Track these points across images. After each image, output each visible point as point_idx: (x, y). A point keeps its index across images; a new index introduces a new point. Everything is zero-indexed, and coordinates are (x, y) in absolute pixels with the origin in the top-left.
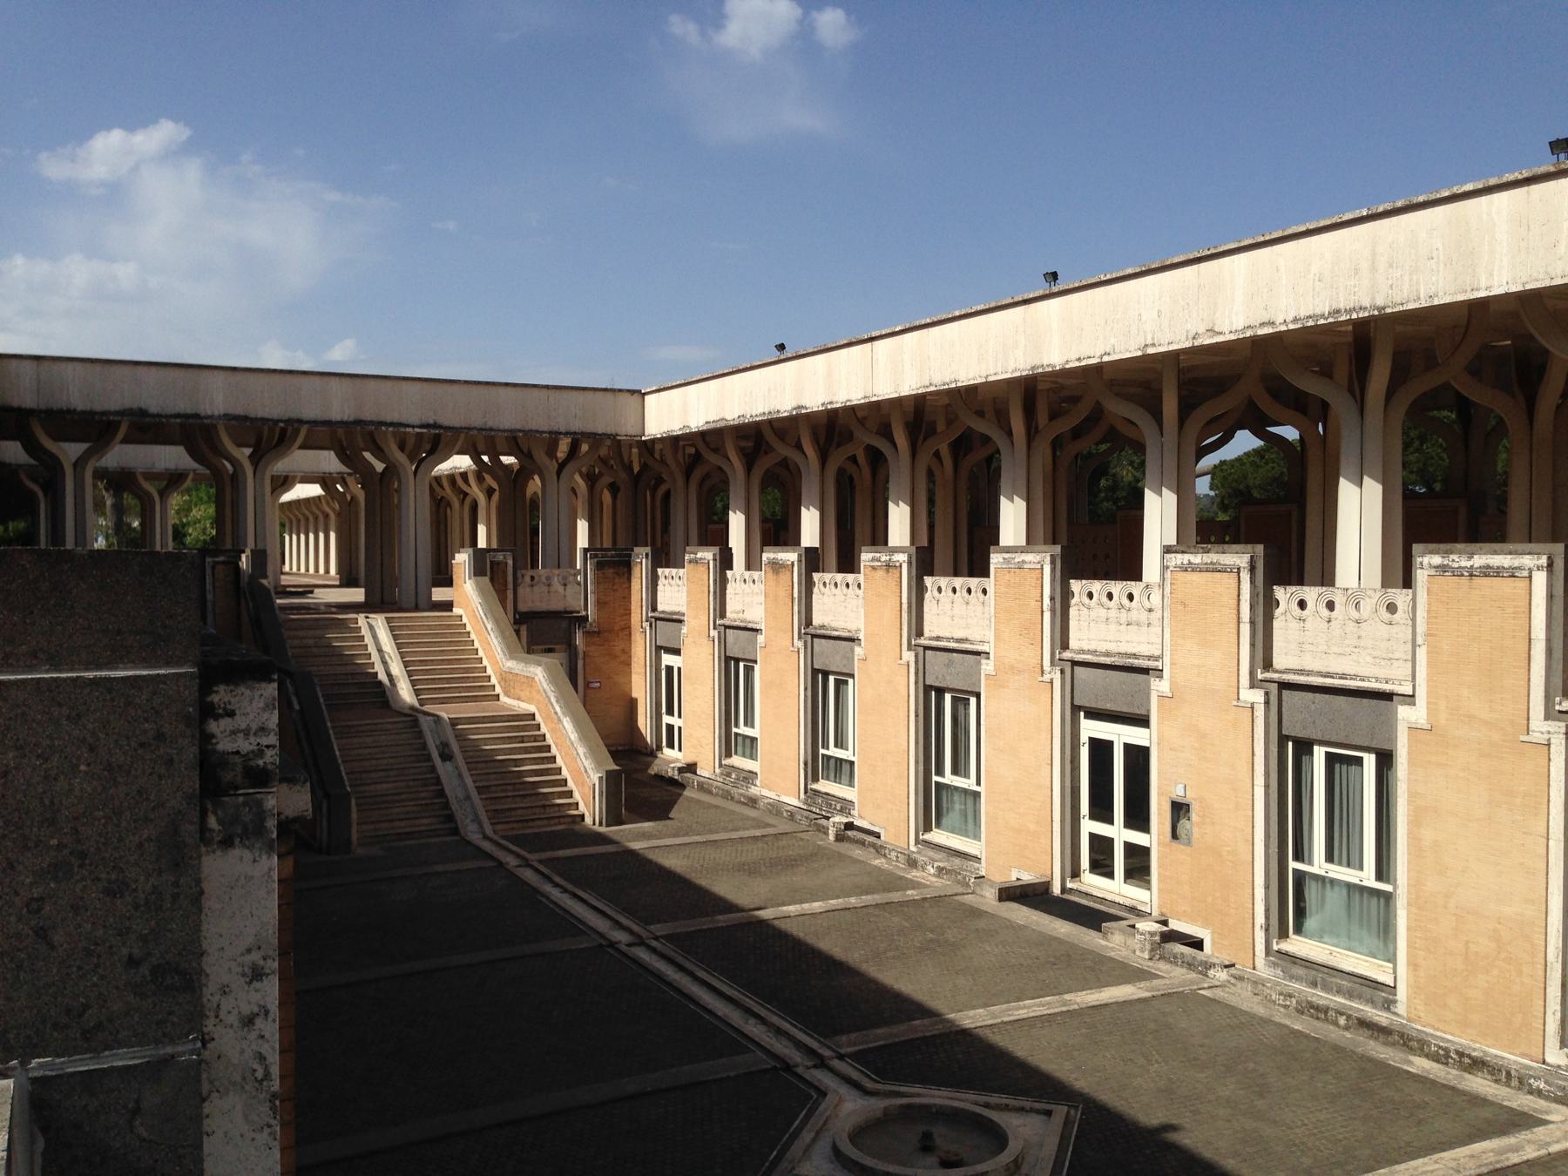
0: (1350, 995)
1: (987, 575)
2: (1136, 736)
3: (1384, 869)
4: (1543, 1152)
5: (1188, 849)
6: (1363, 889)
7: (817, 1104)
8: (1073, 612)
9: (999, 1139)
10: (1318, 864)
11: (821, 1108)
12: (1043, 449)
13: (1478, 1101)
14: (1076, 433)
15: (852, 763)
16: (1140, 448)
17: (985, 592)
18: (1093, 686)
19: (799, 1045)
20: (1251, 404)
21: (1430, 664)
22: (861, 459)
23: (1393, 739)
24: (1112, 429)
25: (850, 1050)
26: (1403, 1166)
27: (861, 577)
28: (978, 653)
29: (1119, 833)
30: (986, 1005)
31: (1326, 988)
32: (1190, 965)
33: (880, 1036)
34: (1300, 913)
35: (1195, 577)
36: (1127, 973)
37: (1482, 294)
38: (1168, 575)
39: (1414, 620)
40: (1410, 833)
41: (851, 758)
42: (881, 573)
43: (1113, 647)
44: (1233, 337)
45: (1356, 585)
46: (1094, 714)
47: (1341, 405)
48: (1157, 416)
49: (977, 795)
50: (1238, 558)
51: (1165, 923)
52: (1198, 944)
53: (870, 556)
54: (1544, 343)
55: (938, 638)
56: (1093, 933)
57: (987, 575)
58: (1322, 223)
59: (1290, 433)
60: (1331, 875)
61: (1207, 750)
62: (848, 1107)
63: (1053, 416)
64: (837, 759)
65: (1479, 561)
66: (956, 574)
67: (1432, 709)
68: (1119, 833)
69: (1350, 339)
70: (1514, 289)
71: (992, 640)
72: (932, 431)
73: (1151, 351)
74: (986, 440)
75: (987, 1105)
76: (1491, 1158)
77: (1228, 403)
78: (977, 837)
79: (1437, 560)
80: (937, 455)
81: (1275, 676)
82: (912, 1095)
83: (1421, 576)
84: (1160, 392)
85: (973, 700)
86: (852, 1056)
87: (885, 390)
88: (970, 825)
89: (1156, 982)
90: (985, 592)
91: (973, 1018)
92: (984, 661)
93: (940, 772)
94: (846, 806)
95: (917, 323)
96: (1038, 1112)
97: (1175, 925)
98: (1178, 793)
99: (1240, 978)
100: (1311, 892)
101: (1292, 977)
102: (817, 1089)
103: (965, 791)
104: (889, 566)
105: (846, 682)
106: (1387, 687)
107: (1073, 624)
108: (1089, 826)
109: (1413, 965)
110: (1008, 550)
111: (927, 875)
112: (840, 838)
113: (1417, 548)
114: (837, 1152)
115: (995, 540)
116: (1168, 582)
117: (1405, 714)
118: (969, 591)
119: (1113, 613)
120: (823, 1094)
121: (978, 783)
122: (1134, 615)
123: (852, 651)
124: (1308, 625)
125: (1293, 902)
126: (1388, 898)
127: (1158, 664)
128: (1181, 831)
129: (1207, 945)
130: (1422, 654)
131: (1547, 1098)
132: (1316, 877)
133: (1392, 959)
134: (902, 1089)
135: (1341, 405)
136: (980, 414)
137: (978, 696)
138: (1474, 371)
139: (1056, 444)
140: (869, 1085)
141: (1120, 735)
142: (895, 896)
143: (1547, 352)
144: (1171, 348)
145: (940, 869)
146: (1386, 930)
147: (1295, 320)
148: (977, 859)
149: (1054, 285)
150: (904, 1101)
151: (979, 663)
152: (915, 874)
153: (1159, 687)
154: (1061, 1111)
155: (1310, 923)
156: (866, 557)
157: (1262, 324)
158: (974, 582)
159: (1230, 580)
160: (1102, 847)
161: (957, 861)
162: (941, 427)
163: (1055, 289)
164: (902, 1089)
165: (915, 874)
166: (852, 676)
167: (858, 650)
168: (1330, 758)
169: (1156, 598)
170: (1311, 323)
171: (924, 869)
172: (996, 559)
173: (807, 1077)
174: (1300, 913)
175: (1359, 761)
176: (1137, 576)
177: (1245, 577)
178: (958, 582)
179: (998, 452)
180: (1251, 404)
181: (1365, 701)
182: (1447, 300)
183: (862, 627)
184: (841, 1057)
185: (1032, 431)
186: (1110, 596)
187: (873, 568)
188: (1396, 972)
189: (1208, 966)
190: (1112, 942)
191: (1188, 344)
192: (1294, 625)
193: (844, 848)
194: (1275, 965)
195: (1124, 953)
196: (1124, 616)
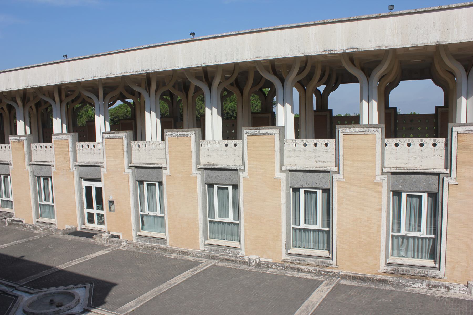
0: (156, 242)
1: (52, 142)
2: (98, 184)
3: (162, 211)
4: (202, 269)
5: (114, 213)
6: (157, 216)
7: (16, 300)
8: (78, 152)
9: (73, 296)
10: (147, 212)
11: (17, 301)
12: (64, 105)
13: (188, 261)
14: (73, 101)
15: (12, 201)
16: (93, 106)
17: (51, 147)
18: (91, 173)
19: (7, 286)
20: (121, 93)
21: (170, 159)
22: (5, 108)
23: (238, 180)
24: (84, 100)
25: (24, 283)
26: (172, 279)
27: (10, 145)
28: (50, 165)
29: (95, 211)
30: (63, 263)
31: (150, 242)
32: (117, 243)
33: (33, 278)
34: (143, 224)
35: (111, 140)
36: (102, 247)
37: (177, 68)
38: (104, 140)
39: (165, 148)
40: (167, 201)
41: (11, 200)
42: (17, 143)
43: (90, 161)
44: (117, 76)
45: (150, 140)
46: (86, 180)
47: (144, 94)
48: (98, 97)
49: (53, 206)
50: (122, 134)
51: (109, 233)
52: (118, 237)
53: (13, 138)
54: (190, 80)
55: (37, 162)
56: (90, 239)
57: (52, 142)
58: (42, 64)
59: (131, 101)
60: (150, 214)
61: (119, 186)
62: (26, 299)
63: (67, 96)
64: (6, 201)
65: (179, 133)
66: (39, 142)
67: (171, 171)
68: (95, 211)
69: (145, 77)
70: (184, 67)
71: (54, 161)
72: (29, 100)
73: (95, 78)
74: (46, 102)
75: (68, 289)
76: (191, 273)
77: (116, 93)
78: (54, 218)
79: (170, 133)
80: (31, 107)
81: (134, 165)
82: (45, 291)
83: (166, 137)
84: (98, 89)
85: (50, 179)
86: (25, 285)
87: (13, 87)
88: (52, 214)
89: (109, 249)
90: (51, 147)
91: (62, 267)
92: (52, 167)
93: (41, 201)
94: (11, 215)
95: (23, 67)
96: (82, 287)
97: (112, 233)
98: (110, 198)
99: (130, 244)
100: (145, 219)
101: (142, 241)
102: (15, 296)
103: (49, 205)
104: (19, 141)
105: (7, 177)
106: (160, 166)
107: (78, 155)
108: (87, 211)
109: (170, 233)
110: (57, 135)
111: (40, 231)
112: (10, 224)
113: (165, 130)
114: (24, 311)
115: (52, 132)
116: (104, 142)
117: (165, 172)
118: (46, 147)
119: (89, 151)
120: (17, 297)
121: (53, 203)
122: (95, 151)
123: (9, 167)
124: (140, 151)
125: (142, 221)
126: (163, 217)
127: (103, 164)
128: (112, 209)
129: (121, 237)
130: (168, 157)
131: (201, 257)
132: (146, 215)
133: (165, 232)
134: (42, 290)
135: (144, 94)
136: (44, 95)
137: (51, 177)
138: (174, 87)
139: (68, 104)
140: (32, 292)
141: (94, 185)
142: (31, 238)
143: (190, 82)
144: (101, 78)
145: (44, 229)
146: (163, 225)
147: (133, 72)
148: (55, 224)
149: (66, 58)
150: (43, 293)
151: (51, 168)
152: (36, 231)
153: (103, 170)
154: (88, 286)
155: (145, 226)
156: (11, 138)
157: (125, 73)
158: (47, 144)
159: (120, 140)
160: (91, 216)
161: (49, 226)
162: (32, 99)
163: (66, 60)
164: (42, 290)
165: (36, 231)
166: (10, 175)
167: (11, 167)
168: (148, 185)
169: (100, 147)
170: (137, 73)
171: (39, 229)
172: (53, 137)
173: (11, 294)
174: (143, 224)
175: (155, 185)
176: (95, 141)
177: (124, 139)
178: (42, 144)
179: (51, 106)
180: (121, 93)
181: (155, 169)
182: (169, 69)
183: (12, 160)
184: (21, 286)
185: (61, 101)
186: (88, 146)
187: (14, 142)
188: (167, 236)
189: (121, 242)
190: (97, 240)
191: (105, 77)
192: (137, 151)
193: (12, 227)
194: (138, 239)
195: (99, 243)
196: (92, 152)
